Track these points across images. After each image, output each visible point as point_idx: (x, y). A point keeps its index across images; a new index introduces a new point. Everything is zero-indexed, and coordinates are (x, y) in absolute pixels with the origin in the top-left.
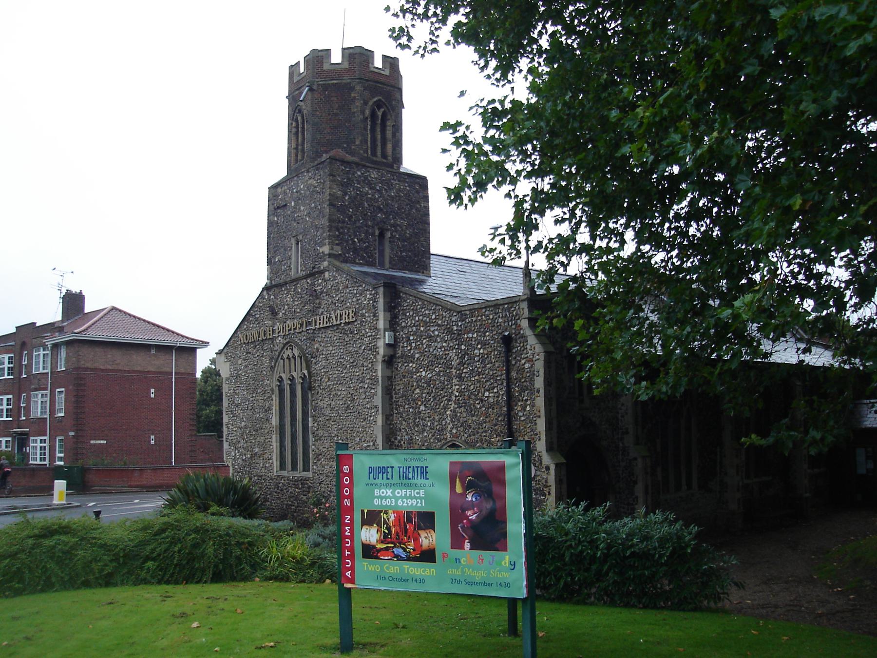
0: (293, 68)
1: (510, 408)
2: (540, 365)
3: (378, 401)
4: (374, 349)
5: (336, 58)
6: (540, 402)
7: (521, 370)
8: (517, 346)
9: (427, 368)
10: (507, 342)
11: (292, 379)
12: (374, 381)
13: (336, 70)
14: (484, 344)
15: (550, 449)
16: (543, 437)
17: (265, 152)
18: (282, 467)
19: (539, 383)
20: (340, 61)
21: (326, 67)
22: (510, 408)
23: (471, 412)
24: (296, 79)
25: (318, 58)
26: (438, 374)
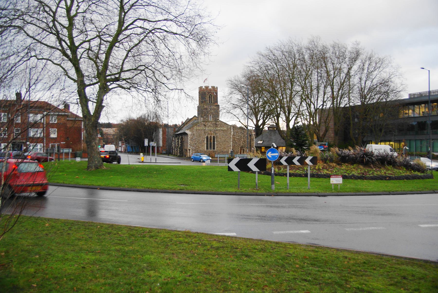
3: (206, 142)
4: (231, 134)
5: (204, 87)
11: (211, 137)
23: (245, 142)
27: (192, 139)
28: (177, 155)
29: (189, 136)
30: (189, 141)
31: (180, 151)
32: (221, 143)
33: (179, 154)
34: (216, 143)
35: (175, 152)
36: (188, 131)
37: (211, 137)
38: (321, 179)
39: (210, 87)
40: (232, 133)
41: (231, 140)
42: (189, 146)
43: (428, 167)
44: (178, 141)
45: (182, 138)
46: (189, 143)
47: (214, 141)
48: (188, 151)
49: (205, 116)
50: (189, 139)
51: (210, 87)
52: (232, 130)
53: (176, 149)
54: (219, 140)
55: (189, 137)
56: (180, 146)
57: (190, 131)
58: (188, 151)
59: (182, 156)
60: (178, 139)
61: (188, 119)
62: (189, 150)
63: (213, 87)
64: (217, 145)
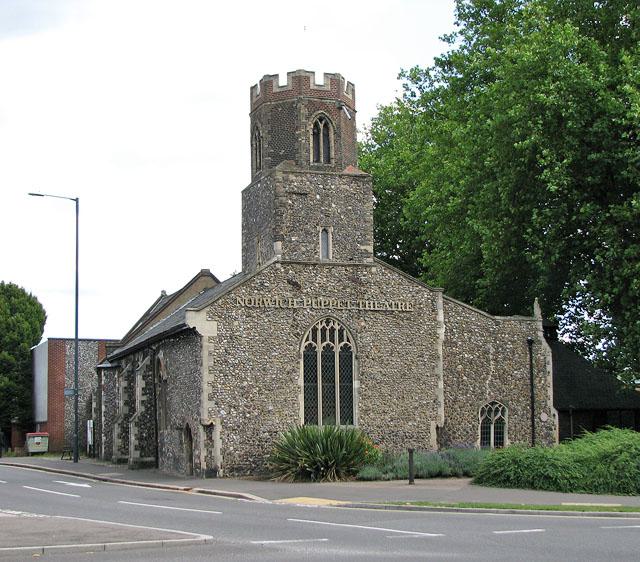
0: (253, 88)
1: (532, 379)
2: (550, 359)
3: (301, 382)
4: (435, 336)
5: (283, 81)
6: (550, 379)
7: (537, 361)
8: (535, 347)
9: (471, 351)
10: (530, 342)
11: (328, 350)
12: (434, 357)
13: (284, 92)
14: (513, 342)
15: (555, 405)
16: (552, 399)
17: (233, 165)
18: (311, 417)
19: (550, 368)
20: (286, 84)
21: (276, 90)
22: (532, 379)
23: (504, 381)
24: (255, 100)
25: (268, 81)
26: (479, 357)
27: (221, 361)
28: (121, 461)
29: (207, 347)
30: (207, 378)
31: (140, 438)
32: (385, 390)
33: (134, 455)
34: (356, 384)
35: (109, 444)
36: (203, 315)
37: (328, 350)
38: (366, 483)
39: (319, 80)
40: (441, 332)
41: (440, 371)
42: (207, 405)
43: (625, 456)
44: (130, 390)
45: (155, 365)
46: (207, 389)
47: (347, 378)
48: (202, 436)
49: (292, 230)
50: (207, 362)
51: (319, 80)
52: (441, 317)
53: (117, 430)
54: (376, 370)
55: (205, 353)
56: (140, 409)
57: (212, 316)
58: (202, 436)
59: (155, 465)
60: (131, 379)
61: (163, 295)
62: (209, 428)
63: (335, 79)
64: (365, 397)
